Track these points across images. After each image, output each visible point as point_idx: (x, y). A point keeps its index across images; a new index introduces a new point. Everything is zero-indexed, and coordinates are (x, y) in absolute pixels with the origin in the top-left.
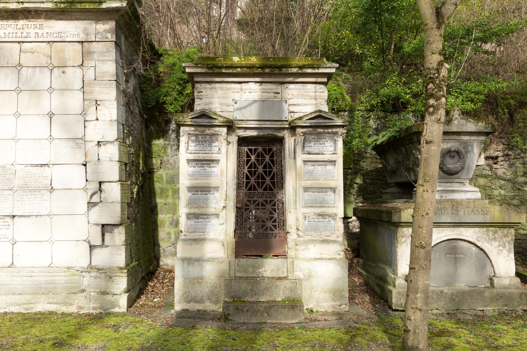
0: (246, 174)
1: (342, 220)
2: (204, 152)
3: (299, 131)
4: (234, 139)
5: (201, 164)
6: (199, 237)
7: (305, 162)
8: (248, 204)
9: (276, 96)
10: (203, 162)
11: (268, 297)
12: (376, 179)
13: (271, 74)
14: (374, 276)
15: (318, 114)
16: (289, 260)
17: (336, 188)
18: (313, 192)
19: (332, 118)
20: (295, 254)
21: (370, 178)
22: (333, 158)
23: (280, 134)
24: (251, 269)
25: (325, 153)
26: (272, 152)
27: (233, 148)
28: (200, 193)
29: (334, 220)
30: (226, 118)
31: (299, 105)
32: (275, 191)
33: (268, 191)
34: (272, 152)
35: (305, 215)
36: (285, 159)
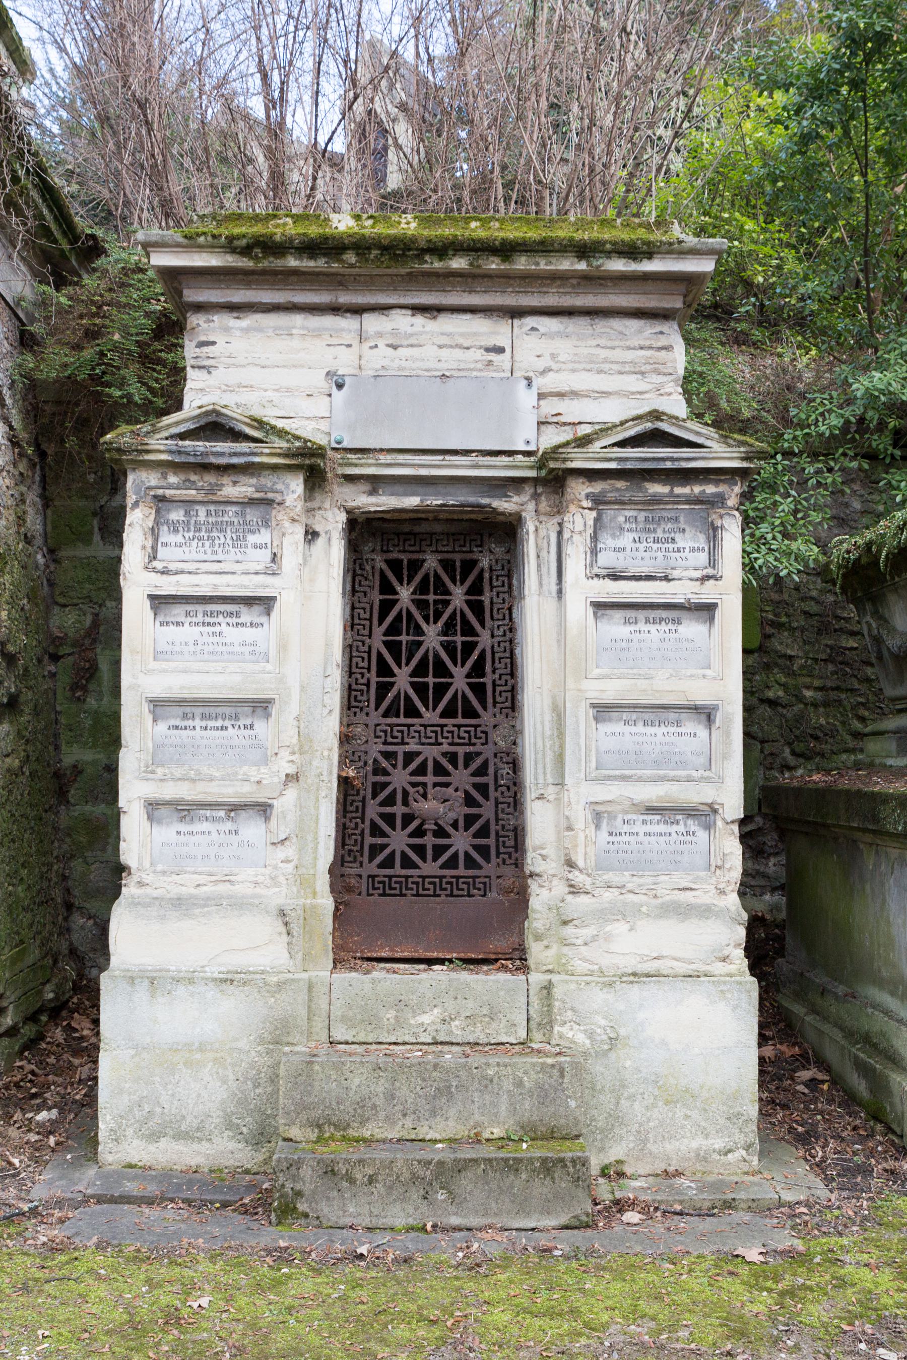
0: (380, 655)
1: (736, 828)
2: (216, 567)
3: (579, 489)
4: (333, 523)
5: (205, 614)
6: (193, 891)
7: (600, 607)
8: (385, 764)
9: (490, 363)
10: (210, 607)
11: (451, 1123)
12: (837, 688)
13: (474, 276)
14: (841, 1029)
15: (649, 425)
16: (536, 978)
17: (715, 708)
18: (626, 723)
19: (700, 440)
20: (559, 956)
21: (817, 683)
22: (707, 593)
23: (505, 505)
24: (391, 1014)
25: (675, 574)
26: (475, 573)
27: (333, 553)
28: (198, 723)
29: (709, 827)
30: (298, 438)
31: (574, 394)
32: (487, 718)
33: (460, 720)
34: (475, 573)
35: (600, 808)
36: (522, 597)
